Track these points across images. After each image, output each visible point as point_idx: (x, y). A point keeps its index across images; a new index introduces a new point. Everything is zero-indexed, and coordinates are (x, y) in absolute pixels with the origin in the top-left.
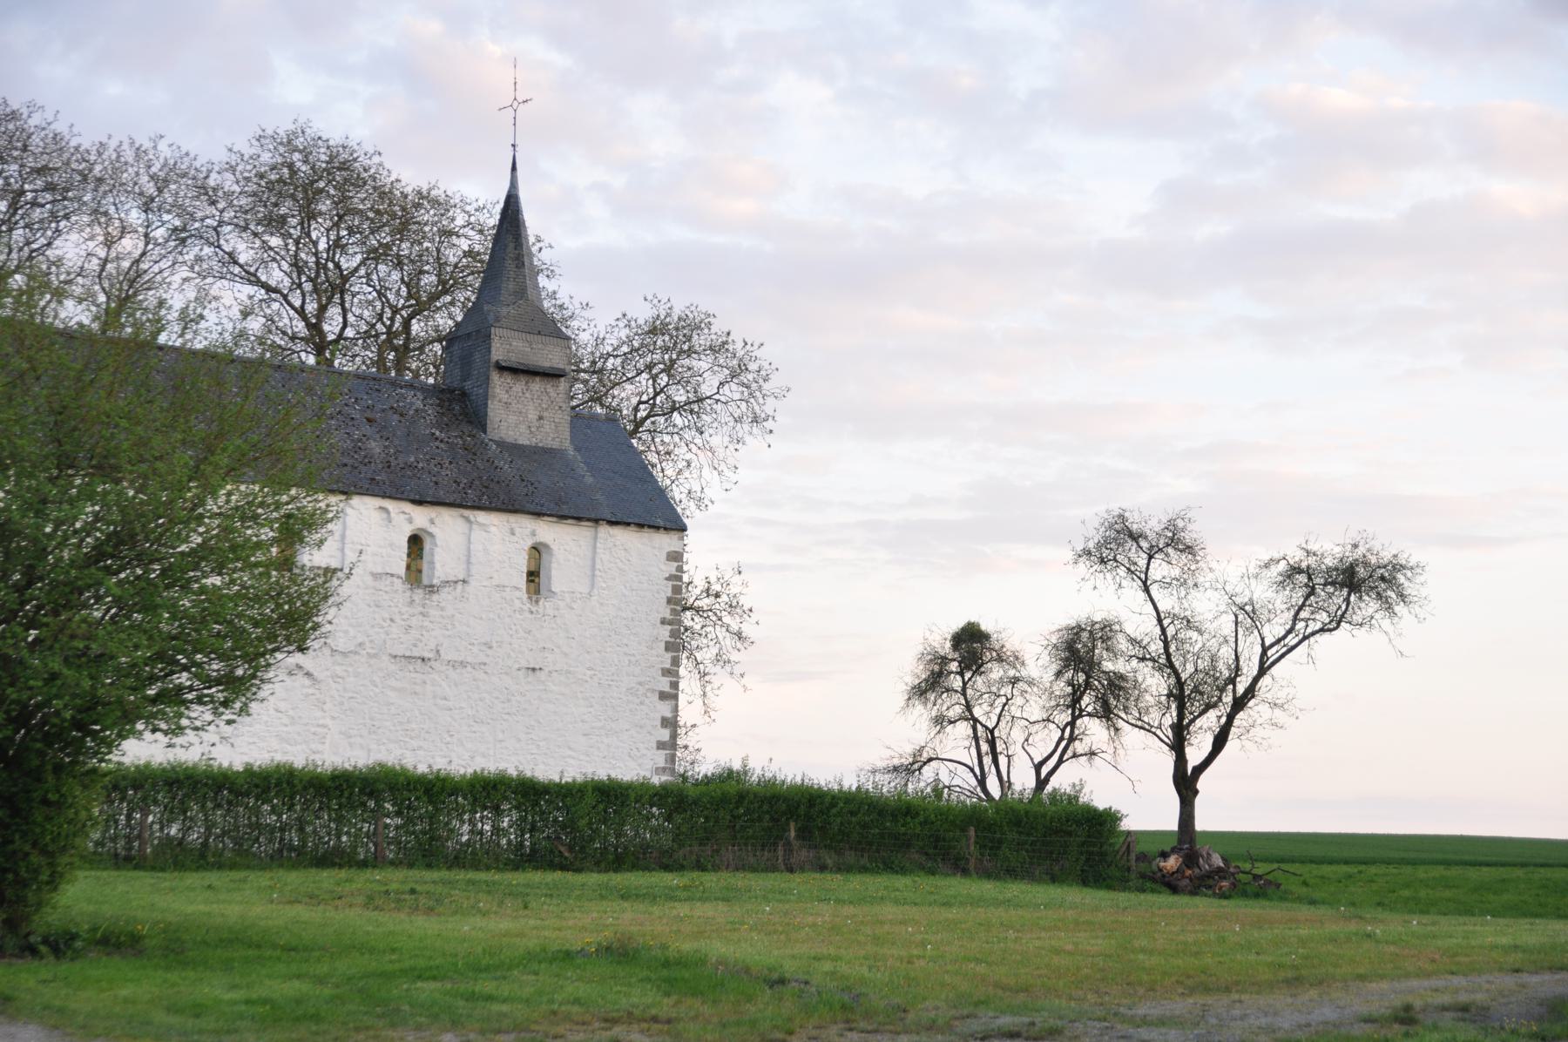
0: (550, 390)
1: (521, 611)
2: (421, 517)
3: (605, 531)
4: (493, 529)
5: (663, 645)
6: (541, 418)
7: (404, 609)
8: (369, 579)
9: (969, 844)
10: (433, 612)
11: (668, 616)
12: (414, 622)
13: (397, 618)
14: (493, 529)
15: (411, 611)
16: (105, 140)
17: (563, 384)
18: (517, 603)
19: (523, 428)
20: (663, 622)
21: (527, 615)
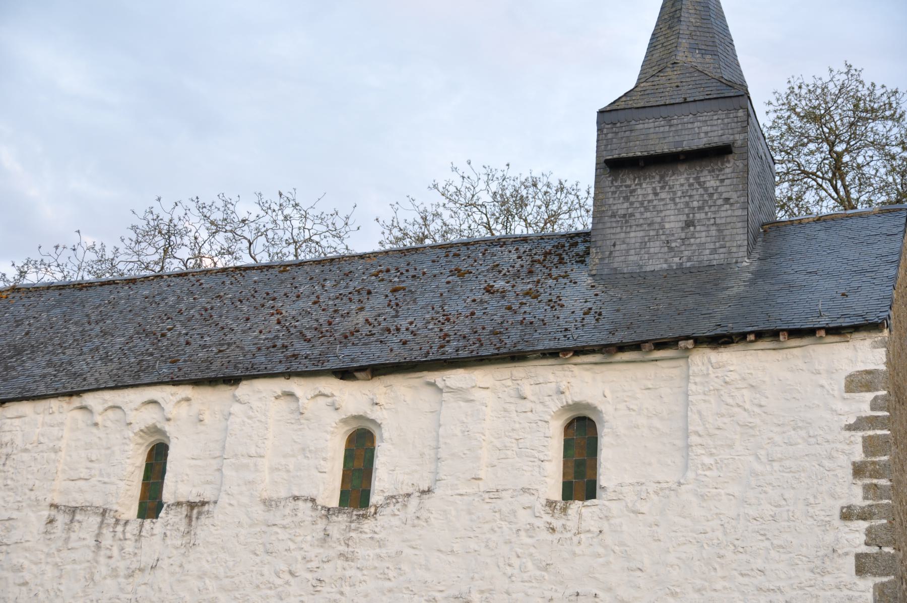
0: (711, 183)
1: (531, 529)
2: (354, 397)
3: (704, 360)
4: (478, 394)
5: (851, 562)
6: (689, 224)
7: (312, 553)
8: (258, 511)
9: (358, 464)
10: (361, 551)
11: (858, 500)
12: (328, 571)
13: (299, 568)
14: (478, 394)
15: (324, 552)
16: (789, 86)
17: (730, 167)
18: (524, 517)
19: (655, 247)
20: (847, 514)
21: (546, 536)
